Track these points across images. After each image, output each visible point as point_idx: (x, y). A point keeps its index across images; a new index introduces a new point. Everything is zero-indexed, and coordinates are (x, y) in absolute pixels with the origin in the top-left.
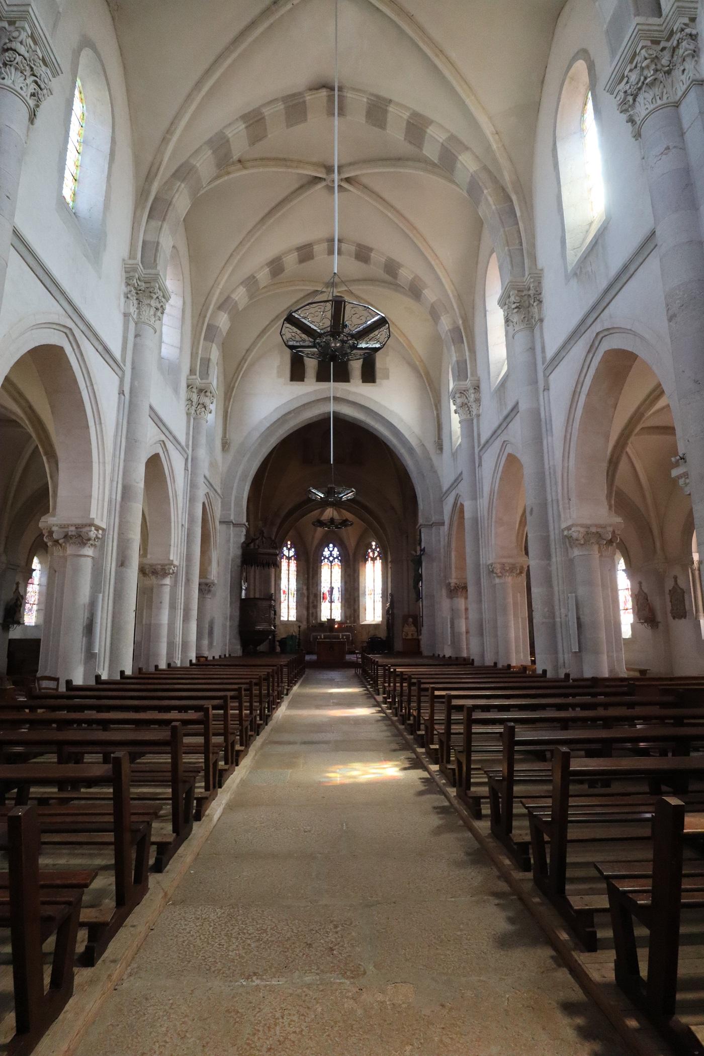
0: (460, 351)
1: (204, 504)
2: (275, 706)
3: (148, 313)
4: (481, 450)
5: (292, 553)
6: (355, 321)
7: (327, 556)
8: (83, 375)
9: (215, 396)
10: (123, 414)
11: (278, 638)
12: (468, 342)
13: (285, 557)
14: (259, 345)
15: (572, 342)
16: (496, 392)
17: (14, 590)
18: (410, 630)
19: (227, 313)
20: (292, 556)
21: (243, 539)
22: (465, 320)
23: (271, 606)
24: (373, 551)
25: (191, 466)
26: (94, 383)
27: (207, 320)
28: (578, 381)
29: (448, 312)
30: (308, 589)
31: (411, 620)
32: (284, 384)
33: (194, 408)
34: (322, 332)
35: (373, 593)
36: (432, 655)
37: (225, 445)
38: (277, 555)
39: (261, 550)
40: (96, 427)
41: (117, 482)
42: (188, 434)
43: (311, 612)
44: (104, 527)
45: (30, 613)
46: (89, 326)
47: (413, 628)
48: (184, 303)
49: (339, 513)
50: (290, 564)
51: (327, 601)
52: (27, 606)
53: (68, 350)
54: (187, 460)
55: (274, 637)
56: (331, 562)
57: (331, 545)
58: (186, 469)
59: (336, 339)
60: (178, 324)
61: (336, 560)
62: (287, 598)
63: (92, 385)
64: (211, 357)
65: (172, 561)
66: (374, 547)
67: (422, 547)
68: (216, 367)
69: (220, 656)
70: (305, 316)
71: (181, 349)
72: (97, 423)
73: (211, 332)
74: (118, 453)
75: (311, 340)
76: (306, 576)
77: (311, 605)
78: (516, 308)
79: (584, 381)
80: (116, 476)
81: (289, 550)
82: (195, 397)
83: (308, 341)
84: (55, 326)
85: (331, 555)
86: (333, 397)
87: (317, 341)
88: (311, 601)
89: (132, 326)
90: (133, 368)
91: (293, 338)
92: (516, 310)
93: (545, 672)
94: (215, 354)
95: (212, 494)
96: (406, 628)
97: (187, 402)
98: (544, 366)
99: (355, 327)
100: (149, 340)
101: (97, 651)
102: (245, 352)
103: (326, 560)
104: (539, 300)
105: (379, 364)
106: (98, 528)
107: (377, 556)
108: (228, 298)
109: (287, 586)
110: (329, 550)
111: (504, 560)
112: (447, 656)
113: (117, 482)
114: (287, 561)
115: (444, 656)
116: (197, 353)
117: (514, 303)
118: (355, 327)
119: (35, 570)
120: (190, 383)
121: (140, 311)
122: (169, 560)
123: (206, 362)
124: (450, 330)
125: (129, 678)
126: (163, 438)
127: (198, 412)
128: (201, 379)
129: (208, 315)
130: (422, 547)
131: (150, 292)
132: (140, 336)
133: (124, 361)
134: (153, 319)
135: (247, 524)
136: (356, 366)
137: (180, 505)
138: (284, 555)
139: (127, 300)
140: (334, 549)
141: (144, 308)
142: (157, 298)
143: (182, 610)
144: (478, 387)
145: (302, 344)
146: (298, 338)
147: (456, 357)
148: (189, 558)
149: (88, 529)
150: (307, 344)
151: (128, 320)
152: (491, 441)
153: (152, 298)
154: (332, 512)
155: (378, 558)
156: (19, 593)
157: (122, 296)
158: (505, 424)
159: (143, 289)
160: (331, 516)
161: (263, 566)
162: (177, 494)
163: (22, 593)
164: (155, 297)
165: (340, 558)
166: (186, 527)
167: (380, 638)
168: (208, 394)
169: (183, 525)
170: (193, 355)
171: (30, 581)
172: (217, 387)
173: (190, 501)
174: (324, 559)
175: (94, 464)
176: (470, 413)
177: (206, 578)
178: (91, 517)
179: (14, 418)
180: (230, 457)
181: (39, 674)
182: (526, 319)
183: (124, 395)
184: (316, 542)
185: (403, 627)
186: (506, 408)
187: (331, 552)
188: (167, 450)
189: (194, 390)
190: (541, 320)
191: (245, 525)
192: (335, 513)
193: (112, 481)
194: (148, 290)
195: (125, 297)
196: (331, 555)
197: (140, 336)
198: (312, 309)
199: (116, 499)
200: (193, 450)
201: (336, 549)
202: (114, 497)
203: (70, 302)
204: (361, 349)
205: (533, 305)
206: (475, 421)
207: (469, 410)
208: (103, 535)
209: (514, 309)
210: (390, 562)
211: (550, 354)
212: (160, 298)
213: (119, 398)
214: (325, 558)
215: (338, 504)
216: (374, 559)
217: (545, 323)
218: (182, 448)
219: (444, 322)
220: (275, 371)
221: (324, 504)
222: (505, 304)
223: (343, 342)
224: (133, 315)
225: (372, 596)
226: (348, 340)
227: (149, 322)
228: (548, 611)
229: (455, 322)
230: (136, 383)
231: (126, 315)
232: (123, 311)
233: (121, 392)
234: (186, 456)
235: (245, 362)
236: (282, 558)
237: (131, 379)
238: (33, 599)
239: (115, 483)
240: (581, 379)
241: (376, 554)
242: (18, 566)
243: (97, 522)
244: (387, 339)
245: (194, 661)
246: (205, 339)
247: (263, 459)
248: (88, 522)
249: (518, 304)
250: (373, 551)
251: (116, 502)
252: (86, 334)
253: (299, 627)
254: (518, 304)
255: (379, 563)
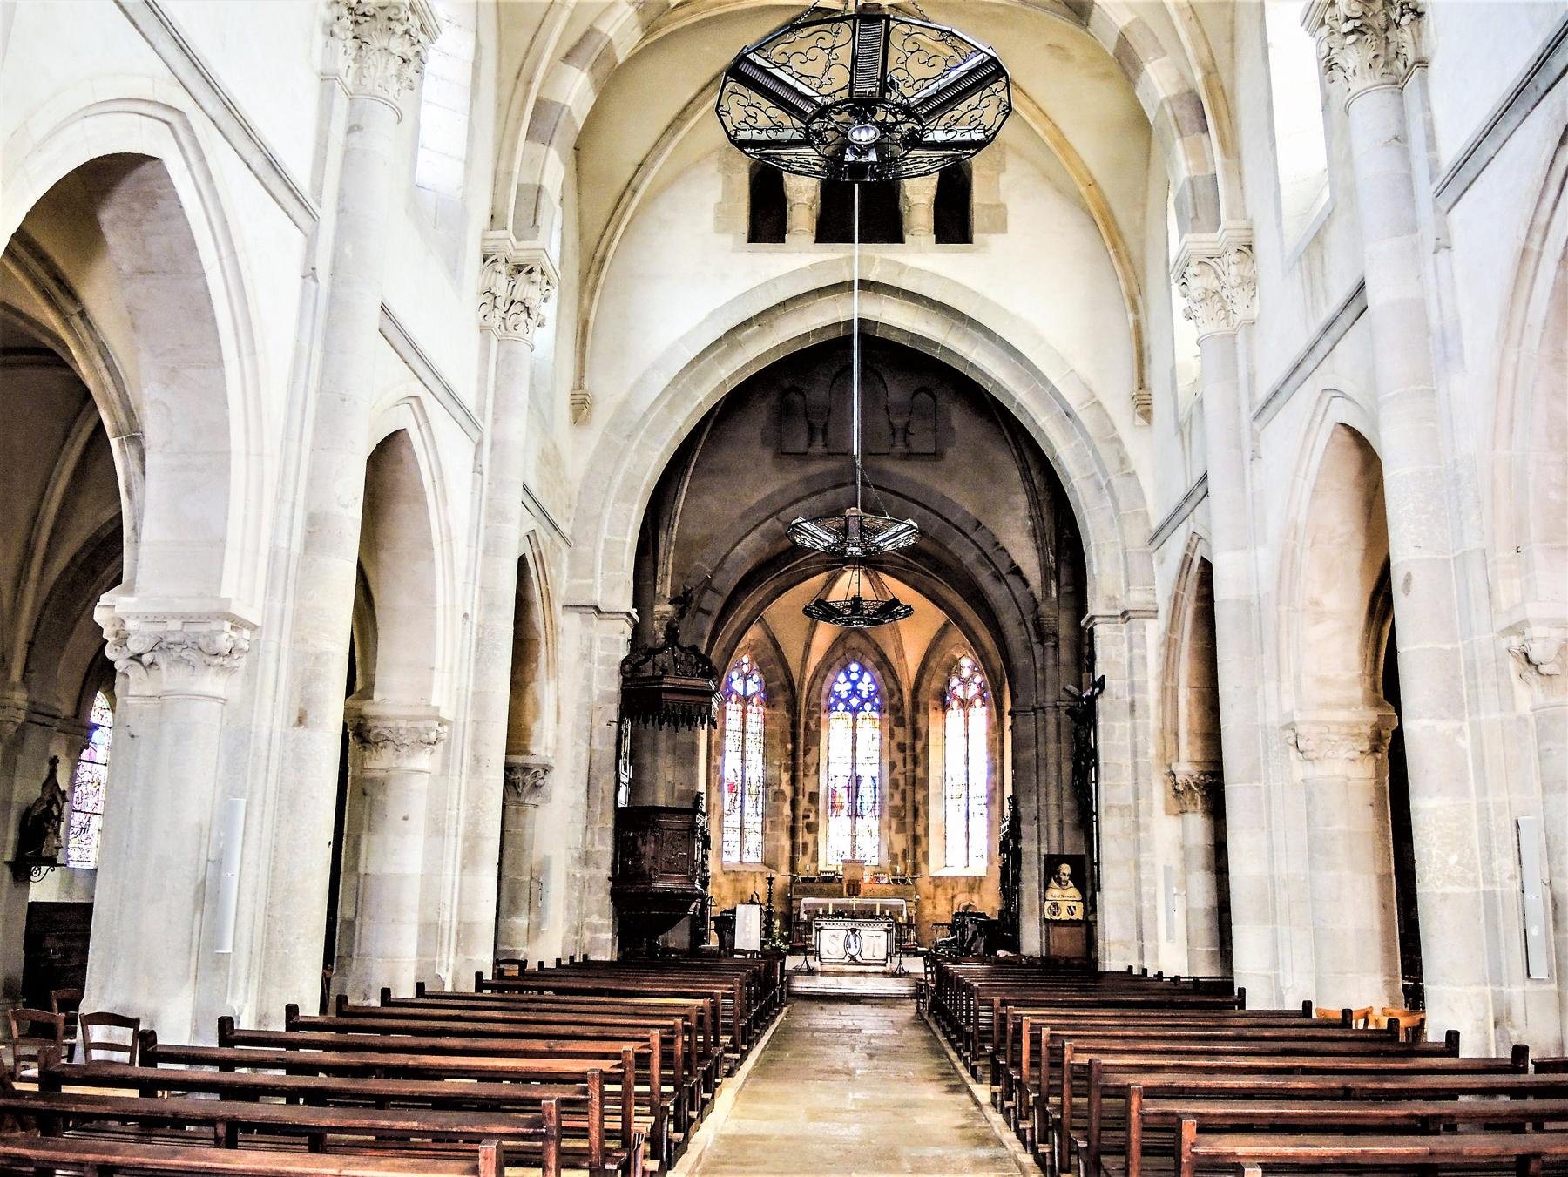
0: (1198, 154)
1: (522, 562)
2: (694, 1114)
3: (382, 70)
4: (1256, 418)
5: (753, 687)
6: (917, 70)
7: (844, 695)
8: (210, 224)
9: (555, 281)
10: (313, 328)
11: (714, 911)
12: (1219, 128)
13: (734, 697)
14: (670, 149)
15: (1514, 118)
16: (1300, 260)
17: (45, 777)
18: (1066, 899)
19: (586, 69)
20: (754, 694)
21: (623, 652)
22: (1210, 72)
23: (693, 828)
24: (965, 682)
25: (491, 461)
26: (237, 249)
27: (535, 87)
28: (1533, 221)
29: (1165, 54)
30: (794, 781)
31: (1065, 869)
32: (733, 251)
33: (499, 313)
34: (829, 101)
35: (965, 793)
36: (1124, 969)
37: (581, 406)
38: (712, 694)
39: (669, 682)
40: (241, 363)
41: (294, 505)
42: (482, 380)
43: (800, 841)
44: (257, 621)
45: (83, 837)
46: (229, 106)
47: (1072, 892)
48: (478, 47)
49: (877, 585)
50: (749, 716)
51: (844, 813)
52: (77, 818)
53: (174, 165)
54: (479, 445)
55: (704, 906)
56: (855, 711)
57: (854, 667)
58: (477, 470)
59: (865, 120)
60: (462, 99)
61: (868, 706)
62: (738, 803)
63: (233, 253)
64: (545, 183)
65: (437, 709)
66: (966, 673)
67: (1097, 678)
68: (559, 209)
69: (558, 961)
70: (783, 59)
71: (468, 163)
72: (244, 351)
73: (543, 118)
74: (296, 429)
75: (798, 124)
76: (789, 746)
77: (801, 824)
78: (1352, 32)
79: (1549, 224)
80: (290, 488)
81: (746, 677)
82: (501, 286)
83: (791, 128)
84: (142, 108)
85: (854, 692)
86: (861, 281)
87: (815, 127)
88: (801, 812)
89: (341, 104)
90: (341, 211)
91: (751, 121)
92: (1352, 38)
93: (1453, 1037)
94: (554, 171)
95: (543, 534)
96: (1054, 892)
97: (483, 299)
98: (1437, 183)
99: (917, 86)
100: (383, 139)
101: (228, 950)
102: (633, 169)
103: (841, 706)
104: (1414, 10)
105: (979, 196)
106: (238, 624)
107: (974, 697)
108: (590, 32)
109: (740, 773)
110: (849, 680)
111: (1327, 716)
112: (1169, 973)
113: (294, 505)
114: (740, 706)
115: (1160, 974)
116: (509, 173)
117: (1348, 19)
118: (917, 86)
119: (96, 727)
120: (489, 249)
121: (360, 68)
122: (428, 706)
123: (533, 196)
124: (1170, 100)
125: (311, 1026)
126: (418, 389)
127: (510, 324)
128: (518, 239)
129: (539, 76)
130: (1097, 678)
131: (390, 19)
132: (359, 128)
133: (318, 190)
134: (394, 86)
135: (633, 612)
136: (919, 194)
137: (461, 563)
138: (731, 692)
139: (331, 40)
140: (861, 676)
141: (373, 59)
142: (406, 32)
143: (460, 841)
144: (1250, 247)
145: (772, 135)
146: (763, 121)
147: (1189, 169)
148: (480, 701)
149: (215, 626)
150: (785, 136)
151: (332, 89)
152: (1285, 392)
153: (394, 33)
154: (855, 579)
155: (978, 702)
156: (57, 784)
157: (318, 30)
158: (1325, 345)
159: (372, 11)
160: (853, 592)
161: (676, 724)
162: (453, 533)
163: (63, 784)
164: (400, 29)
165: (877, 700)
166: (475, 621)
167: (983, 915)
168: (536, 276)
169: (466, 616)
170: (499, 179)
171: (85, 755)
172: (561, 263)
173: (486, 552)
174: (836, 704)
175: (233, 456)
176: (1227, 317)
177: (526, 752)
178: (224, 594)
179: (47, 341)
180: (593, 436)
181: (86, 1007)
182: (1381, 60)
183: (317, 281)
184: (815, 658)
185: (1046, 888)
186: (1327, 304)
187: (854, 683)
188: (427, 422)
189: (500, 267)
190: (1422, 63)
191: (629, 614)
192: (865, 581)
193: (279, 501)
194: (382, 15)
195: (324, 33)
196: (854, 692)
197: (359, 128)
198: (802, 41)
199: (289, 549)
200: (495, 421)
201: (867, 677)
202: (283, 544)
203: (183, 48)
204: (934, 146)
205: (1398, 25)
206: (1240, 339)
207: (1224, 308)
208: (254, 644)
209: (1346, 34)
210: (1011, 713)
211: (1450, 152)
212: (413, 32)
213: (304, 288)
214: (838, 698)
215: (872, 562)
216: (965, 704)
217: (1434, 67)
218: (468, 415)
219: (1154, 78)
220: (708, 217)
221: (836, 561)
222: (1323, 23)
223: (885, 128)
224: (343, 75)
225: (963, 801)
226: (898, 123)
227: (384, 95)
228: (1458, 863)
229: (1182, 78)
230: (348, 250)
231: (325, 77)
232: (318, 68)
233: (310, 273)
234: (476, 436)
235: (633, 196)
236: (727, 697)
237: (336, 238)
238: (91, 801)
239: (287, 508)
240: (1542, 219)
241: (973, 690)
242: (54, 717)
243: (238, 609)
244: (1001, 117)
245: (488, 976)
246: (530, 135)
247: (676, 446)
248: (214, 606)
249: (1358, 23)
250: (965, 682)
251: (289, 557)
252: (222, 125)
253: (770, 880)
254: (1358, 23)
255: (980, 716)
